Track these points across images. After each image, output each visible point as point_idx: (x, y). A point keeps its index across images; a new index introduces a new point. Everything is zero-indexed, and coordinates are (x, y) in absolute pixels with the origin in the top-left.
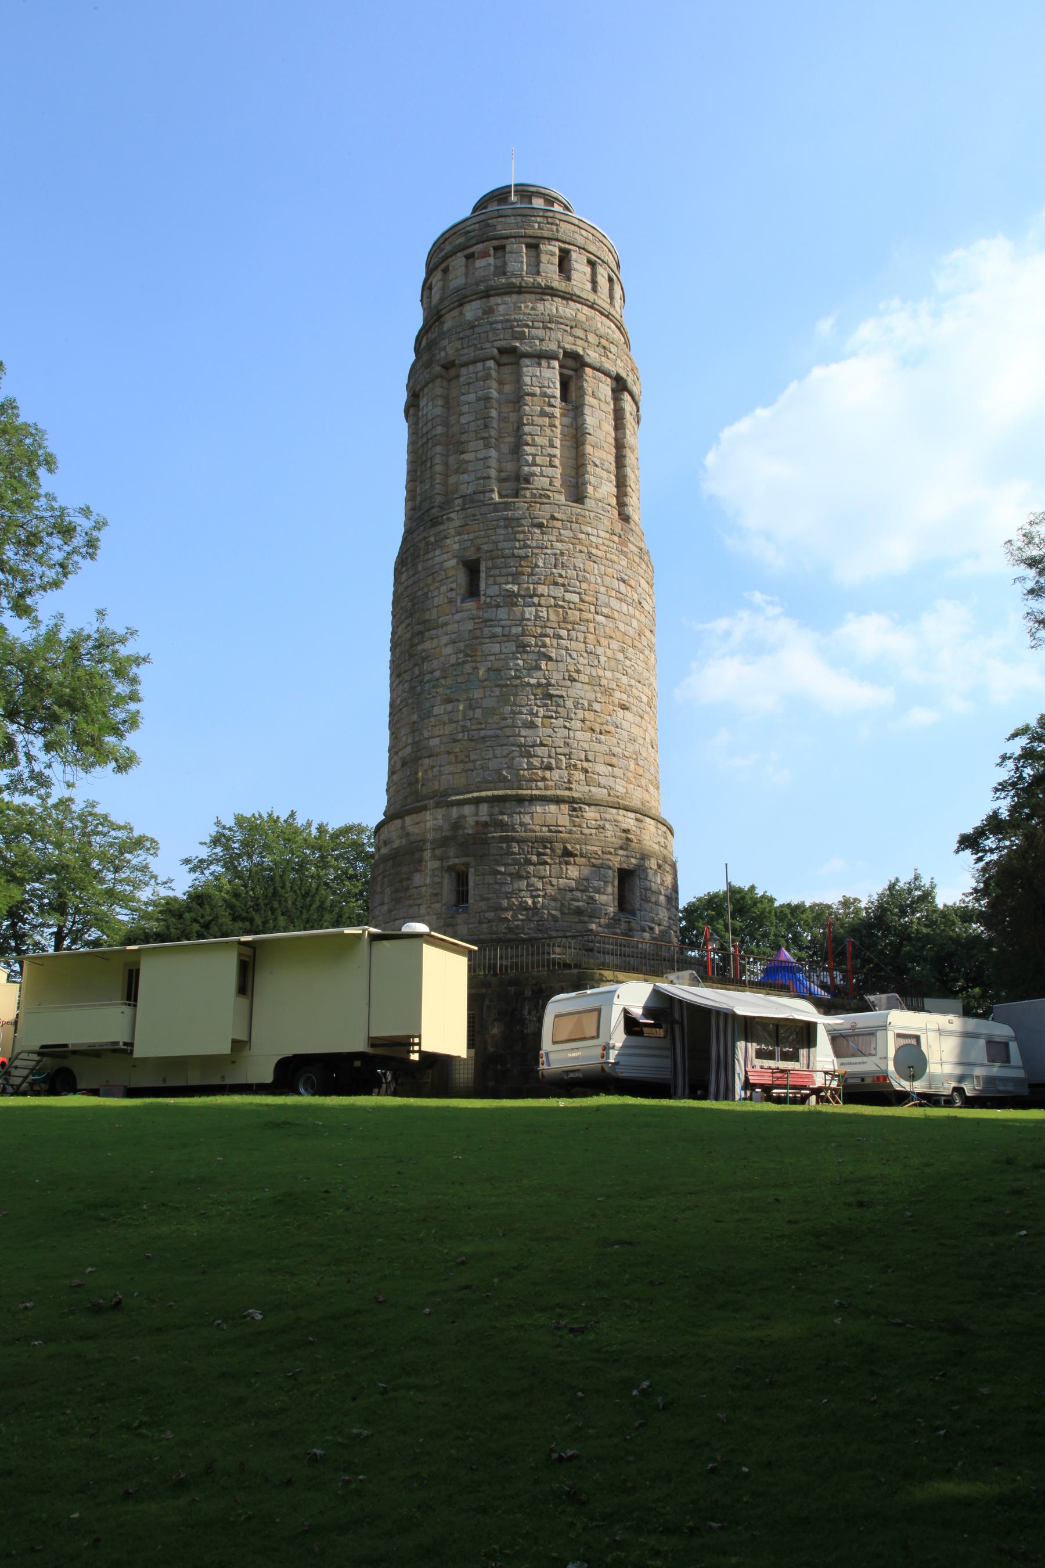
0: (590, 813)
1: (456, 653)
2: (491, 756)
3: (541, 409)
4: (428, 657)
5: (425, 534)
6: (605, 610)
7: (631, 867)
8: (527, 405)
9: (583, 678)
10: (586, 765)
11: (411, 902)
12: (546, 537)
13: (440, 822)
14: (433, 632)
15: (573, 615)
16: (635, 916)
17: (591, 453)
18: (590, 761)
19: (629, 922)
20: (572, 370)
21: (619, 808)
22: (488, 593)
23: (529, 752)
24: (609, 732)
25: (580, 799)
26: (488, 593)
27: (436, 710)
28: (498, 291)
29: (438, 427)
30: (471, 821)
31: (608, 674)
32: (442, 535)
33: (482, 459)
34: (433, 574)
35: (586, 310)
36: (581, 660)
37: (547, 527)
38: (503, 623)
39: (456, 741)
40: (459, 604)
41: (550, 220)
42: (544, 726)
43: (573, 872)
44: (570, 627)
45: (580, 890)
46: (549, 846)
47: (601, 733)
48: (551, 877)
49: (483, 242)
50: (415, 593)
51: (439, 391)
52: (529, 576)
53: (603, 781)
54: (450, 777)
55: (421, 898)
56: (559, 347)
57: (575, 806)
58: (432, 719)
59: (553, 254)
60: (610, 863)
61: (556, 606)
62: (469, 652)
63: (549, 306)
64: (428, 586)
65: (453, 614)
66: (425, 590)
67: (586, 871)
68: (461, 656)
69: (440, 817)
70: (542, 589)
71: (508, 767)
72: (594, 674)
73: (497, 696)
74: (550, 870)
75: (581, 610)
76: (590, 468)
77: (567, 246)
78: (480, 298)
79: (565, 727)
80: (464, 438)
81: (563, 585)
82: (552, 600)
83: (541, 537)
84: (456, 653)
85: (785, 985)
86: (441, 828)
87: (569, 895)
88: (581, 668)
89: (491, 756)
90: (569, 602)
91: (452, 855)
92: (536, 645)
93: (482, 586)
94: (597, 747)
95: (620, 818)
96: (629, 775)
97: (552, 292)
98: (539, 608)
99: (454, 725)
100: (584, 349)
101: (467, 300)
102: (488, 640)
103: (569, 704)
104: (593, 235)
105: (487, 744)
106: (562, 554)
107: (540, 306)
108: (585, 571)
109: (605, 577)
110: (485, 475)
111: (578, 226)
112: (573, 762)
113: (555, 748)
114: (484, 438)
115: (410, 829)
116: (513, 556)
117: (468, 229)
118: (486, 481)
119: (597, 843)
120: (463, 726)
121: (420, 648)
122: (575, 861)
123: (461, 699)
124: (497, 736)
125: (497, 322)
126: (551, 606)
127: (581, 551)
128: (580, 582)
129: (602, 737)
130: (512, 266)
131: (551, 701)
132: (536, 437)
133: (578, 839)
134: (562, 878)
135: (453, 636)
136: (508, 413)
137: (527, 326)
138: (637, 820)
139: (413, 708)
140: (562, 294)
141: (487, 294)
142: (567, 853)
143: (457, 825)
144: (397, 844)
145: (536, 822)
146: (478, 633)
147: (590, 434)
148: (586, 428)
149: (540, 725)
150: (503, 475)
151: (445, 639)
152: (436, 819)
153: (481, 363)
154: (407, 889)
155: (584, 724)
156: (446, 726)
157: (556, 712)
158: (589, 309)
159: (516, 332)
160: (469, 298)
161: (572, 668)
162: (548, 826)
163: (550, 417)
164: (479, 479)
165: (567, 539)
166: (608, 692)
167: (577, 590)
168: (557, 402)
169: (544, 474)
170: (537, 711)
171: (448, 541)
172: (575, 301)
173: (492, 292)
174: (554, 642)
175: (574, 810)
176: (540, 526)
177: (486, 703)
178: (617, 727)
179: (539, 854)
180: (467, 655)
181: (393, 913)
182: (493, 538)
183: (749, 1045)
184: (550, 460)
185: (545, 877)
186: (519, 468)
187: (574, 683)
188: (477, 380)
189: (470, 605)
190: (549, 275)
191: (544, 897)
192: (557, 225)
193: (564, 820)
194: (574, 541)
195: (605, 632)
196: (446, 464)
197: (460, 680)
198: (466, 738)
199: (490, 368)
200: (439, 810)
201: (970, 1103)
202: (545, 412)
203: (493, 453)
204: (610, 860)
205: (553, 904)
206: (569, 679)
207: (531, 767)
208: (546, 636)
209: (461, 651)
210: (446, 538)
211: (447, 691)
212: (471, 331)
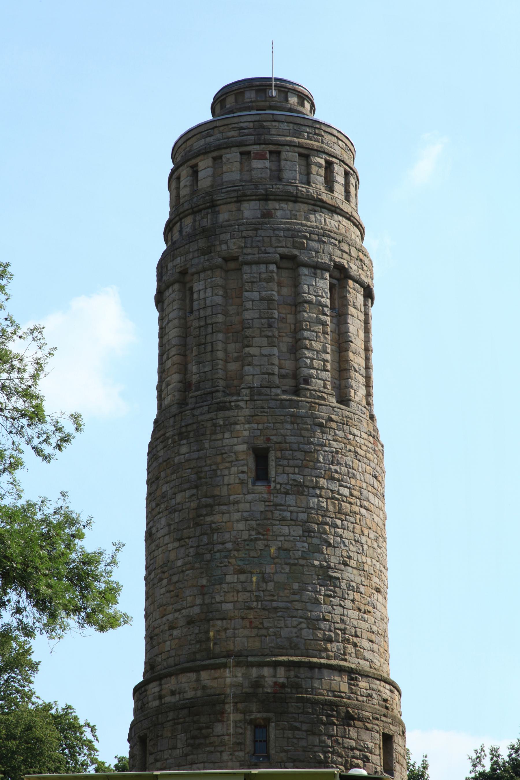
0: (363, 684)
1: (249, 530)
2: (283, 625)
3: (317, 316)
4: (218, 529)
5: (212, 415)
6: (366, 504)
8: (306, 311)
9: (353, 563)
10: (356, 640)
11: (212, 749)
13: (240, 680)
14: (224, 508)
15: (346, 506)
16: (393, 776)
17: (353, 359)
18: (359, 637)
20: (336, 279)
22: (278, 481)
25: (356, 670)
26: (278, 481)
27: (229, 578)
28: (277, 197)
29: (220, 316)
30: (270, 681)
31: (369, 560)
32: (232, 420)
33: (266, 356)
34: (222, 454)
35: (345, 222)
36: (352, 548)
37: (326, 427)
38: (292, 508)
39: (250, 608)
40: (250, 486)
41: (317, 131)
42: (325, 603)
44: (343, 517)
47: (365, 613)
49: (260, 144)
50: (201, 467)
51: (219, 280)
53: (367, 654)
54: (245, 640)
55: (224, 745)
56: (331, 260)
58: (225, 586)
59: (320, 166)
61: (333, 498)
62: (261, 531)
63: (319, 218)
64: (217, 464)
65: (245, 494)
66: (214, 467)
68: (253, 533)
69: (240, 675)
73: (287, 573)
74: (337, 731)
75: (350, 503)
76: (352, 373)
78: (259, 200)
79: (341, 605)
80: (248, 332)
83: (321, 436)
84: (249, 530)
86: (241, 685)
88: (351, 554)
89: (283, 625)
91: (254, 709)
92: (319, 531)
93: (272, 473)
94: (363, 624)
95: (381, 689)
97: (334, 210)
98: (321, 499)
99: (248, 594)
101: (245, 198)
102: (278, 522)
103: (344, 585)
104: (346, 145)
105: (279, 614)
108: (353, 469)
109: (365, 474)
110: (270, 371)
112: (347, 636)
113: (334, 623)
114: (268, 337)
115: (209, 683)
116: (300, 450)
117: (242, 125)
118: (271, 376)
119: (369, 710)
120: (257, 596)
121: (208, 519)
122: (354, 724)
123: (254, 571)
124: (287, 608)
125: (279, 229)
127: (350, 451)
128: (350, 478)
129: (365, 616)
130: (286, 175)
131: (330, 581)
132: (313, 342)
135: (245, 514)
136: (286, 314)
137: (305, 237)
139: (202, 573)
140: (329, 207)
141: (266, 198)
143: (257, 684)
144: (190, 694)
145: (324, 687)
146: (269, 515)
147: (352, 342)
148: (350, 336)
149: (322, 602)
150: (283, 371)
151: (237, 516)
152: (236, 677)
153: (264, 265)
154: (206, 737)
155: (354, 604)
156: (240, 594)
157: (334, 592)
158: (347, 221)
159: (297, 242)
160: (248, 198)
161: (345, 554)
163: (323, 325)
164: (264, 373)
166: (369, 577)
167: (348, 485)
168: (327, 310)
169: (320, 377)
170: (320, 590)
171: (238, 427)
173: (271, 197)
174: (333, 530)
177: (277, 578)
178: (374, 608)
179: (328, 716)
180: (259, 533)
181: (188, 757)
182: (282, 431)
184: (324, 365)
185: (333, 736)
186: (298, 368)
187: (347, 567)
188: (260, 281)
189: (261, 488)
190: (318, 186)
192: (322, 136)
193: (344, 687)
196: (225, 351)
197: (253, 554)
198: (259, 606)
199: (272, 272)
200: (239, 669)
202: (320, 319)
203: (275, 351)
204: (377, 725)
206: (343, 564)
208: (327, 524)
209: (253, 529)
210: (236, 423)
211: (240, 563)
212: (255, 232)
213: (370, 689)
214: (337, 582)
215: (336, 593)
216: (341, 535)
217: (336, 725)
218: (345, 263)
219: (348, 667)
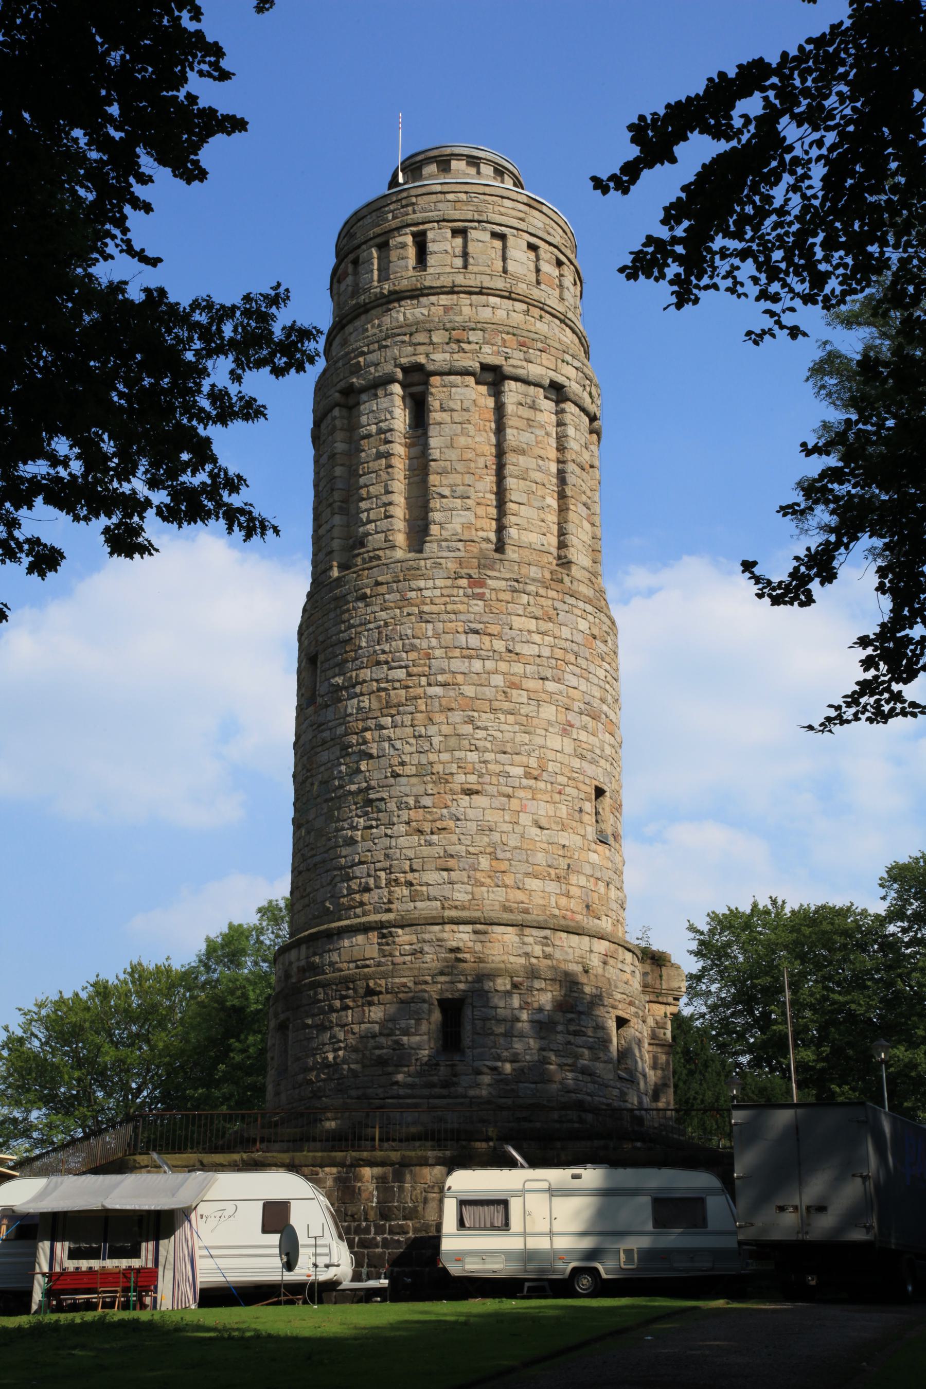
0: (404, 937)
6: (440, 678)
7: (457, 995)
9: (410, 770)
10: (410, 876)
12: (369, 610)
18: (416, 871)
19: (453, 1066)
21: (444, 923)
23: (348, 873)
24: (444, 829)
36: (408, 749)
37: (371, 596)
41: (404, 202)
42: (364, 840)
43: (376, 1013)
44: (393, 711)
45: (384, 1035)
46: (352, 986)
47: (432, 833)
48: (353, 1023)
52: (353, 661)
53: (433, 891)
57: (385, 931)
60: (426, 995)
61: (379, 690)
67: (392, 1009)
70: (366, 674)
71: (332, 896)
72: (424, 761)
75: (407, 687)
77: (421, 227)
81: (387, 663)
82: (375, 684)
87: (371, 1043)
88: (406, 758)
90: (393, 681)
94: (426, 851)
96: (479, 875)
100: (427, 355)
103: (392, 806)
104: (466, 193)
106: (386, 624)
107: (386, 319)
111: (441, 193)
112: (393, 876)
113: (374, 863)
119: (408, 973)
126: (373, 692)
127: (409, 614)
128: (406, 652)
129: (435, 837)
133: (383, 972)
134: (364, 1023)
140: (408, 294)
142: (370, 992)
149: (359, 839)
155: (410, 826)
157: (377, 820)
158: (450, 296)
161: (395, 761)
162: (355, 961)
163: (386, 457)
165: (392, 605)
166: (444, 779)
167: (403, 664)
172: (428, 295)
173: (344, 322)
174: (376, 733)
176: (364, 597)
178: (458, 820)
179: (342, 998)
183: (58, 1246)
185: (346, 1025)
187: (398, 779)
191: (345, 1048)
192: (413, 204)
194: (401, 604)
195: (441, 705)
201: (604, 1288)
204: (426, 991)
205: (354, 1056)
206: (392, 776)
207: (351, 892)
213: (419, 942)
214: (382, 805)
215: (380, 820)
216: (389, 737)
217: (352, 1008)
218: (422, 359)
219: (376, 922)
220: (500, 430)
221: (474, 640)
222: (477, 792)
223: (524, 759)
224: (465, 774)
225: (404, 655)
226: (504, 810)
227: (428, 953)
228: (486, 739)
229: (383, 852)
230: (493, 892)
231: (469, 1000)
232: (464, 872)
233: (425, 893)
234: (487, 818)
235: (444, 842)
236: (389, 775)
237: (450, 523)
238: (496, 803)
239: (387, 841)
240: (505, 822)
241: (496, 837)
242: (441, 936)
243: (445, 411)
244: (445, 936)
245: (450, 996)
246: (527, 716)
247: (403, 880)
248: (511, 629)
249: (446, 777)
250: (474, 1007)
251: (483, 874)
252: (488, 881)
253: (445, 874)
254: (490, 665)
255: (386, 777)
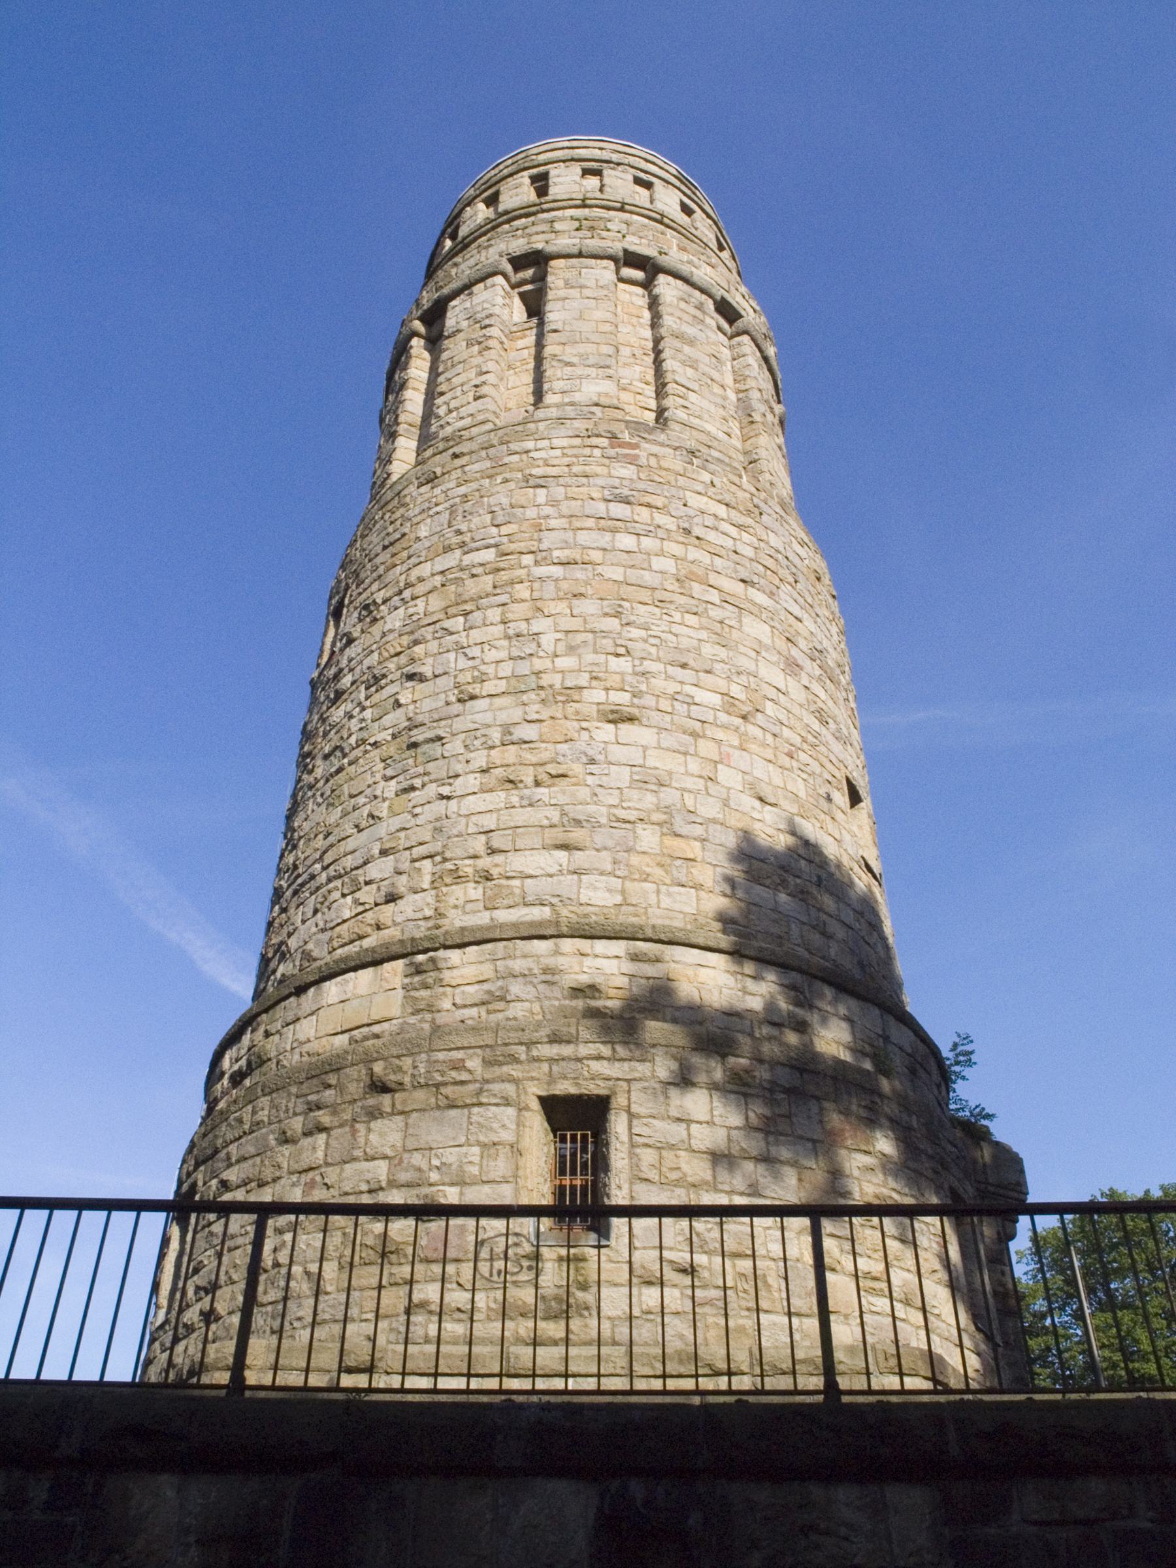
10: (485, 862)
46: (333, 1082)
47: (537, 784)
70: (425, 570)
77: (542, 169)
85: (692, 1190)
94: (522, 816)
96: (635, 860)
134: (355, 1159)
138: (635, 958)
140: (522, 211)
167: (492, 541)
175: (419, 970)
178: (592, 761)
218: (540, 246)
220: (656, 321)
221: (618, 510)
222: (631, 719)
223: (722, 685)
224: (607, 689)
225: (494, 530)
226: (685, 754)
227: (519, 1000)
228: (646, 641)
229: (430, 826)
230: (669, 894)
231: (620, 1101)
232: (604, 853)
233: (517, 891)
234: (650, 762)
235: (562, 799)
236: (453, 699)
237: (579, 390)
238: (668, 740)
239: (440, 807)
240: (687, 773)
241: (669, 796)
242: (551, 962)
243: (572, 287)
244: (561, 962)
245: (573, 1090)
246: (721, 622)
247: (470, 870)
248: (685, 505)
249: (568, 692)
250: (631, 1116)
251: (647, 859)
252: (658, 872)
253: (562, 855)
254: (648, 543)
255: (448, 704)
